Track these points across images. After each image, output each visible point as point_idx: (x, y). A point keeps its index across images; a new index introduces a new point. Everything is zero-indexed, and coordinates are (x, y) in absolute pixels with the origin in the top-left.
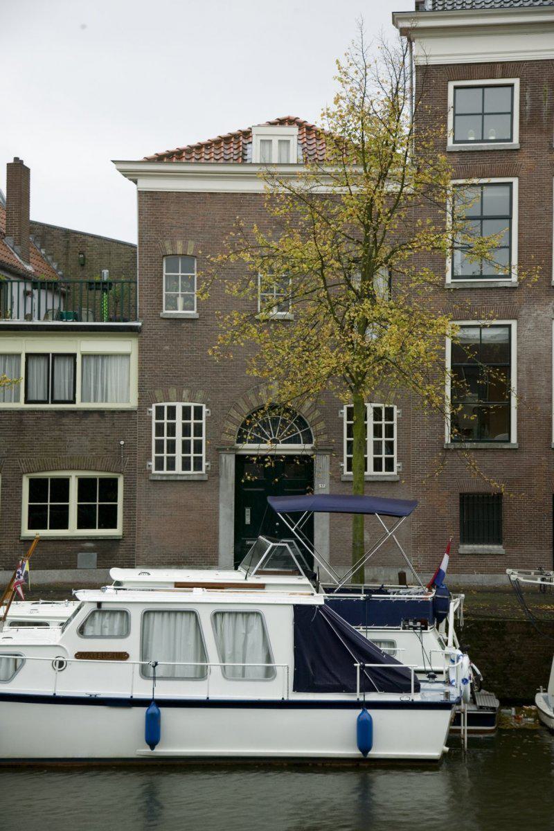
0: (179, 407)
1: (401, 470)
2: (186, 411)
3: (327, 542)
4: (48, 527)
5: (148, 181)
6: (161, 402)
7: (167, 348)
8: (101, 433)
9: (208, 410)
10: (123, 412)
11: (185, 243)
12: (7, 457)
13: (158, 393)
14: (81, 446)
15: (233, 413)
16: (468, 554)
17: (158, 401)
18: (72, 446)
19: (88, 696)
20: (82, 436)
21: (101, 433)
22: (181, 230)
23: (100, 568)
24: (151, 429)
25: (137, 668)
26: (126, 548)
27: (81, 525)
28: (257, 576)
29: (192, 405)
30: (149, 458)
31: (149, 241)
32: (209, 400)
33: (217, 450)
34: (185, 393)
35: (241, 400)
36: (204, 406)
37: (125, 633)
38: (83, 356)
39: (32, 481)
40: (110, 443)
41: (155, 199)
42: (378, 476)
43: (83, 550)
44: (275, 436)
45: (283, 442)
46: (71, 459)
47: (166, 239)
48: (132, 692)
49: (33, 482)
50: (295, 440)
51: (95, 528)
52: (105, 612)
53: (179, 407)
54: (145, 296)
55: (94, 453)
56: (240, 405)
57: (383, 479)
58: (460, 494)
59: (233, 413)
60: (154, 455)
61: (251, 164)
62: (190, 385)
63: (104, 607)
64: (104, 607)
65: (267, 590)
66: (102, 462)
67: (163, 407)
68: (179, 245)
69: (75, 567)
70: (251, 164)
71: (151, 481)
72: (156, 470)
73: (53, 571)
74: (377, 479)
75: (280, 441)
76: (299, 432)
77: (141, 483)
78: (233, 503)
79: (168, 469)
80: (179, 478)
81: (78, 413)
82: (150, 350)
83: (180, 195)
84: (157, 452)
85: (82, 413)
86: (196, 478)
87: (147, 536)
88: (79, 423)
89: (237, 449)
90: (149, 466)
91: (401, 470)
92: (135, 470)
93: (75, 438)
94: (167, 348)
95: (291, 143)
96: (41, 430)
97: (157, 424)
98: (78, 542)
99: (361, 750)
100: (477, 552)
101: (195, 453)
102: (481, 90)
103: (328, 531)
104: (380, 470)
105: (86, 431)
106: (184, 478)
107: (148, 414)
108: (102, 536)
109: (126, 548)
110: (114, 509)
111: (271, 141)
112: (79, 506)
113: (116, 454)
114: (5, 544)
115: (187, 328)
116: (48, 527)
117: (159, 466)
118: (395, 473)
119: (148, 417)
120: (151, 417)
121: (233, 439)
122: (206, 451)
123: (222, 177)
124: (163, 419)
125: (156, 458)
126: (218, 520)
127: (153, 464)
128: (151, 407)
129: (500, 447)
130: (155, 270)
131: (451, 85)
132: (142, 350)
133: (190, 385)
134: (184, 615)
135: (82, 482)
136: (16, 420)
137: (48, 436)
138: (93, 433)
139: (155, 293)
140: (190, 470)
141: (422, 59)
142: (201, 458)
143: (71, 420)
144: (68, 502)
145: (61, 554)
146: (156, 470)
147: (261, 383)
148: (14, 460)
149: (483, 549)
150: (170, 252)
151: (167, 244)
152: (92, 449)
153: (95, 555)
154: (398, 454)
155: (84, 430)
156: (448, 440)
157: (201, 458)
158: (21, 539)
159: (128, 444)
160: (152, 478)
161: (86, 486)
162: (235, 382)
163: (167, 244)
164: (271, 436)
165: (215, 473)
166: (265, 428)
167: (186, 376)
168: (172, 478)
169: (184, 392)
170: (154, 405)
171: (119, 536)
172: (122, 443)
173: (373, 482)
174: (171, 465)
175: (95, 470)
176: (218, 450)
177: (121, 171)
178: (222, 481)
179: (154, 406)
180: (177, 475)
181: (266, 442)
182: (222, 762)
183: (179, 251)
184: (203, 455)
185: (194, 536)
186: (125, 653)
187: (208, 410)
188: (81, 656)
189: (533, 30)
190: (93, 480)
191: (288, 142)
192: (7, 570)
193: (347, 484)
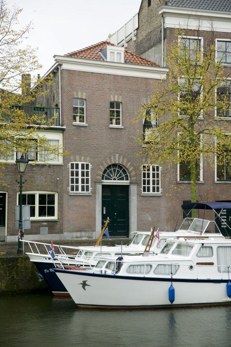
1: (162, 191)
2: (83, 166)
3: (136, 221)
5: (112, 70)
6: (73, 162)
7: (75, 138)
8: (49, 175)
10: (58, 165)
11: (82, 93)
12: (11, 185)
13: (72, 158)
14: (41, 180)
15: (101, 167)
18: (37, 180)
19: (207, 279)
20: (42, 176)
21: (49, 175)
22: (80, 88)
23: (49, 234)
25: (216, 268)
26: (59, 225)
27: (40, 215)
28: (205, 234)
29: (85, 163)
30: (68, 186)
31: (68, 92)
32: (92, 161)
33: (95, 182)
34: (82, 158)
35: (104, 161)
36: (90, 164)
37: (212, 255)
41: (70, 73)
43: (43, 226)
45: (118, 180)
46: (37, 186)
47: (74, 91)
48: (197, 277)
50: (122, 179)
52: (206, 247)
54: (66, 115)
55: (46, 183)
56: (104, 164)
57: (156, 195)
59: (101, 167)
60: (70, 184)
61: (107, 62)
62: (84, 154)
63: (205, 245)
64: (205, 245)
65: (209, 238)
67: (74, 164)
68: (80, 93)
69: (39, 233)
70: (107, 62)
71: (69, 195)
72: (71, 191)
73: (30, 235)
74: (154, 195)
75: (117, 179)
76: (124, 175)
77: (65, 196)
78: (101, 205)
80: (81, 194)
81: (40, 166)
82: (68, 139)
83: (80, 73)
84: (143, 184)
85: (41, 166)
86: (87, 194)
87: (68, 219)
88: (40, 170)
91: (162, 191)
92: (63, 191)
93: (39, 177)
94: (75, 138)
95: (121, 54)
98: (40, 222)
99: (170, 301)
102: (225, 43)
103: (136, 216)
104: (155, 192)
105: (43, 173)
106: (83, 194)
108: (50, 220)
109: (59, 225)
110: (53, 208)
111: (121, 53)
113: (55, 184)
114: (10, 224)
115: (83, 130)
117: (72, 189)
118: (160, 193)
120: (69, 168)
121: (101, 178)
123: (78, 64)
126: (95, 212)
127: (70, 188)
128: (141, 166)
131: (217, 40)
133: (84, 154)
134: (229, 248)
135: (41, 196)
141: (177, 26)
142: (89, 186)
143: (37, 169)
144: (35, 205)
145: (33, 228)
146: (71, 191)
147: (111, 154)
148: (13, 186)
150: (76, 97)
151: (75, 93)
152: (46, 182)
153: (47, 228)
154: (161, 185)
156: (178, 180)
157: (89, 186)
159: (60, 179)
160: (70, 194)
161: (42, 197)
162: (101, 154)
163: (75, 93)
164: (113, 177)
165: (94, 192)
168: (78, 194)
169: (82, 157)
170: (70, 163)
171: (56, 220)
173: (153, 196)
174: (77, 189)
175: (47, 191)
176: (95, 182)
180: (80, 193)
181: (111, 180)
182: (141, 307)
183: (80, 97)
184: (90, 185)
185: (86, 219)
186: (213, 263)
188: (198, 264)
189: (229, 21)
190: (45, 195)
191: (121, 53)
193: (143, 197)
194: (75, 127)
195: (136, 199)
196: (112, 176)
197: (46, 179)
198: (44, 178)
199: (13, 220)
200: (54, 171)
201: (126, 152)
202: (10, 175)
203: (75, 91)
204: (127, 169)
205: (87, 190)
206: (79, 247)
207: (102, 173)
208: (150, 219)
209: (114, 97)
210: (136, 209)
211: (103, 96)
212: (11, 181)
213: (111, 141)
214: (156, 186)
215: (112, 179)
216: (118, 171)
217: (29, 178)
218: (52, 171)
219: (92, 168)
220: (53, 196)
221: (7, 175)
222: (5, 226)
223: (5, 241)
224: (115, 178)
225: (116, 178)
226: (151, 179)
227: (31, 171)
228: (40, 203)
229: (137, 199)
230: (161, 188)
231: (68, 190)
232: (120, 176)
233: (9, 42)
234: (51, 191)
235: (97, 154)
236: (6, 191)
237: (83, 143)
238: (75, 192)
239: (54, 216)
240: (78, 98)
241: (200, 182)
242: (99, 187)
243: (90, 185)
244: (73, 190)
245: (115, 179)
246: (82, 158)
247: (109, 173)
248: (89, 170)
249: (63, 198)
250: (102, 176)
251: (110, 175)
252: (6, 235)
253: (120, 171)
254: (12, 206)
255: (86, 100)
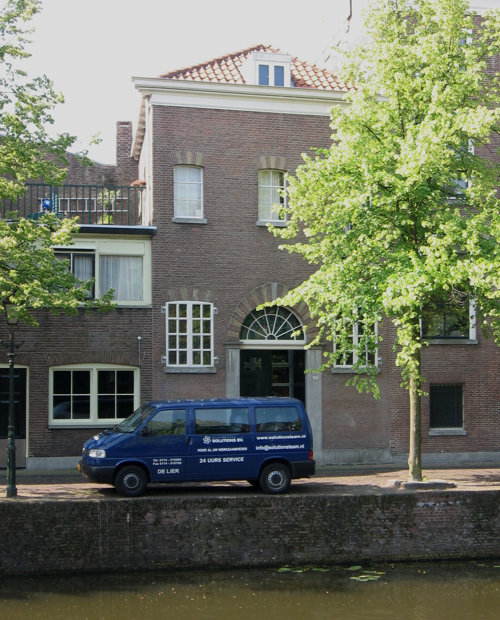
0: (190, 304)
4: (72, 417)
6: (173, 301)
8: (120, 329)
9: (215, 308)
12: (34, 351)
13: (170, 292)
14: (102, 341)
15: (238, 310)
16: (437, 436)
17: (171, 299)
18: (94, 341)
21: (120, 329)
24: (180, 328)
30: (163, 352)
31: (162, 151)
32: (216, 299)
34: (195, 292)
38: (102, 256)
39: (56, 373)
40: (128, 339)
42: (182, 368)
44: (274, 333)
45: (279, 338)
49: (57, 374)
51: (114, 417)
53: (190, 304)
57: (345, 372)
58: (430, 384)
59: (238, 310)
60: (168, 350)
66: (121, 356)
67: (175, 305)
75: (276, 337)
79: (180, 363)
80: (191, 371)
83: (190, 111)
89: (242, 344)
90: (164, 359)
91: (381, 363)
96: (65, 326)
97: (170, 321)
100: (444, 434)
101: (180, 348)
107: (162, 311)
112: (99, 397)
115: (197, 232)
116: (72, 417)
117: (172, 359)
119: (163, 314)
121: (237, 334)
122: (215, 346)
124: (175, 316)
125: (170, 352)
127: (167, 357)
128: (165, 305)
129: (463, 343)
130: (168, 178)
132: (155, 252)
135: (103, 376)
136: (43, 316)
137: (71, 331)
138: (113, 329)
139: (167, 200)
140: (200, 363)
142: (210, 352)
148: (41, 354)
149: (449, 432)
155: (104, 326)
157: (210, 352)
158: (50, 427)
159: (145, 339)
160: (167, 371)
163: (178, 155)
165: (222, 366)
166: (262, 325)
167: (195, 277)
169: (194, 291)
172: (139, 338)
174: (183, 359)
175: (115, 363)
177: (137, 87)
178: (229, 374)
179: (167, 304)
181: (264, 338)
183: (189, 162)
184: (212, 349)
187: (215, 308)
192: (37, 457)
194: (178, 227)
195: (320, 381)
196: (264, 330)
197: (113, 339)
198: (109, 336)
199: (41, 425)
200: (131, 321)
201: (295, 279)
202: (33, 331)
203: (179, 150)
204: (298, 315)
205: (207, 360)
206: (301, 479)
207: (239, 325)
208: (353, 423)
209: (268, 159)
210: (321, 402)
211: (242, 159)
212: (35, 344)
213: (262, 254)
214: (202, 350)
215: (266, 337)
216: (279, 319)
217: (76, 336)
218: (127, 321)
219: (217, 313)
220: (130, 375)
221: (27, 331)
222: (24, 437)
223: (25, 468)
224: (272, 334)
225: (275, 335)
226: (190, 334)
227: (80, 321)
228: (101, 390)
229: (322, 379)
230: (378, 356)
231: (162, 362)
232: (284, 330)
233: (247, 83)
234: (124, 364)
235: (230, 284)
236: (24, 365)
237: (197, 260)
238: (178, 365)
239: (89, 418)
240: (186, 164)
241: (468, 343)
242: (234, 356)
243: (212, 349)
244: (175, 362)
245: (272, 338)
246: (195, 292)
247: (257, 324)
248: (211, 319)
249: (152, 378)
250: (239, 330)
251: (262, 330)
252: (27, 456)
253: (284, 321)
254: (38, 397)
255: (203, 167)
